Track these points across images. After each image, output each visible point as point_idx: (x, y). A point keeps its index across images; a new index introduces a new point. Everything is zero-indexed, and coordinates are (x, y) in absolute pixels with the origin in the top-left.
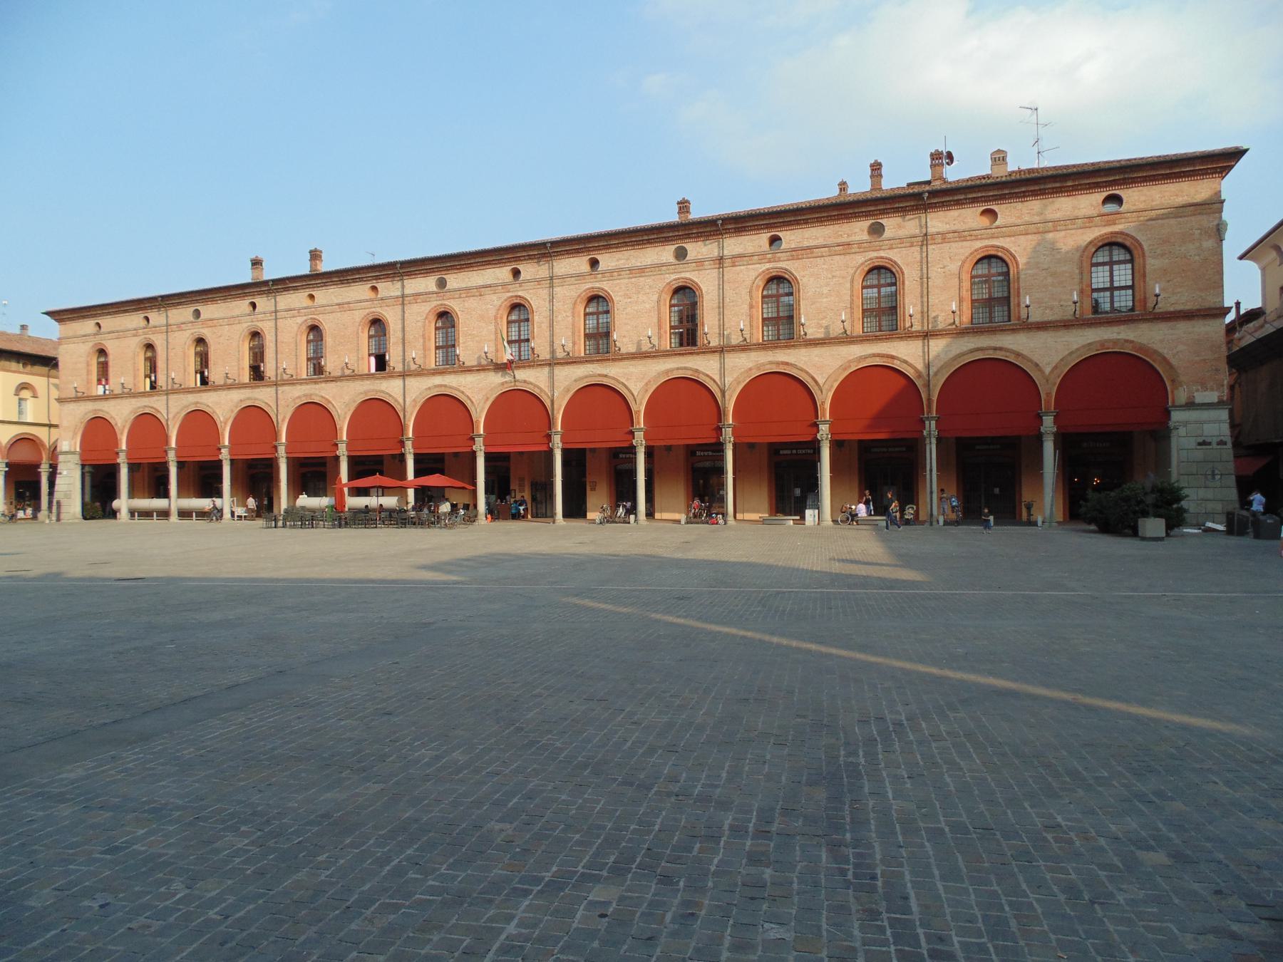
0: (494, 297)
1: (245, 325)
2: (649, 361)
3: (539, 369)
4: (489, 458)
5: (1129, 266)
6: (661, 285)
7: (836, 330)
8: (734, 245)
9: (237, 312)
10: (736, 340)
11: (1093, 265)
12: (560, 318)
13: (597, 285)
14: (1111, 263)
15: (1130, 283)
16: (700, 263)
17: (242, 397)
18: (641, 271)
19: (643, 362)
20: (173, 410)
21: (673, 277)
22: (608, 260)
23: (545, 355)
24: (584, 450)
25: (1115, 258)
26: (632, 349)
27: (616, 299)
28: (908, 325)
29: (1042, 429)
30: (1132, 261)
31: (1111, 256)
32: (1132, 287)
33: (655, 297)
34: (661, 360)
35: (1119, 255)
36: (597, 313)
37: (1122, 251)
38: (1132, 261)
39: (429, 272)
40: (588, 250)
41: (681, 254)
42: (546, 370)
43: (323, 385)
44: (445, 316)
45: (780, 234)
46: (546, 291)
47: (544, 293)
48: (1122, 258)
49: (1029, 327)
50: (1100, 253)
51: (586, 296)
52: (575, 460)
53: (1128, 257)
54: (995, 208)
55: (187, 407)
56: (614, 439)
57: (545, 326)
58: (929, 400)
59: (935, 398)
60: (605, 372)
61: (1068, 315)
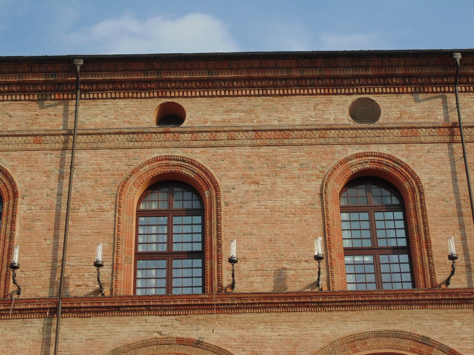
2: (307, 316)
3: (17, 323)
5: (399, 215)
6: (327, 164)
7: (301, 278)
8: (99, 113)
10: (81, 284)
12: (82, 212)
13: (179, 153)
15: (402, 243)
16: (409, 132)
18: (283, 135)
19: (292, 316)
21: (352, 151)
22: (200, 111)
23: (34, 283)
26: (265, 285)
27: (223, 184)
28: (226, 283)
30: (402, 207)
32: (407, 250)
33: (316, 185)
34: (337, 315)
36: (169, 213)
37: (188, 195)
39: (136, 88)
40: (161, 86)
41: (365, 113)
42: (36, 325)
45: (182, 102)
46: (54, 157)
47: (49, 160)
48: (187, 205)
51: (148, 173)
53: (197, 205)
57: (44, 226)
60: (194, 335)
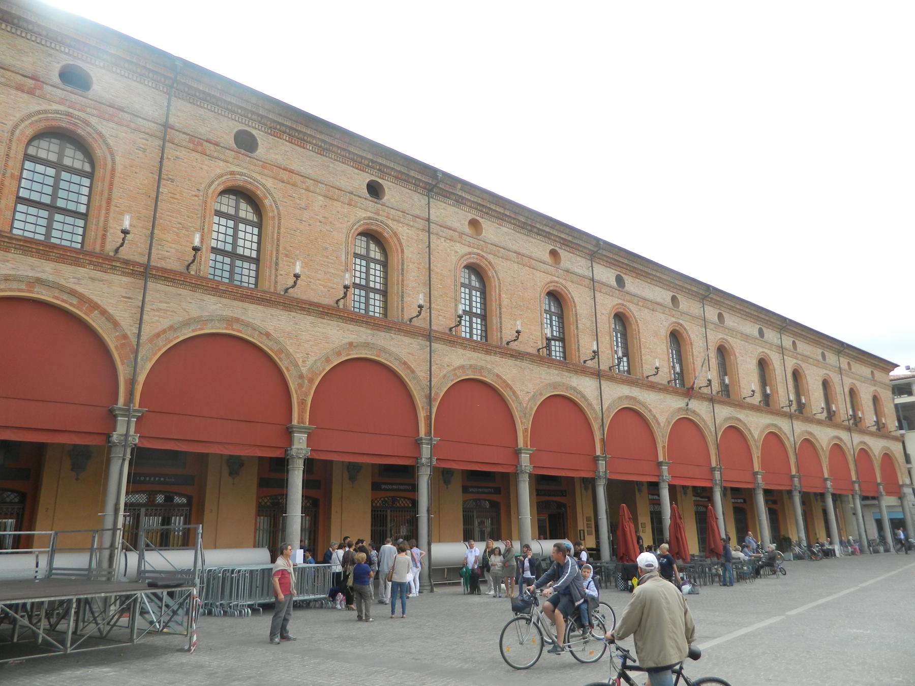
0: (663, 316)
1: (363, 214)
4: (309, 464)
9: (343, 183)
11: (27, 157)
14: (237, 219)
17: (352, 338)
20: (155, 322)
24: (41, 448)
25: (67, 162)
29: (294, 452)
30: (259, 225)
31: (61, 155)
32: (257, 261)
35: (245, 211)
37: (79, 155)
38: (259, 225)
43: (497, 359)
44: (621, 318)
48: (78, 165)
49: (287, 302)
50: (44, 144)
52: (319, 475)
53: (87, 168)
54: (561, 252)
55: (203, 321)
56: (391, 451)
58: (132, 382)
59: (141, 378)
61: (328, 301)
